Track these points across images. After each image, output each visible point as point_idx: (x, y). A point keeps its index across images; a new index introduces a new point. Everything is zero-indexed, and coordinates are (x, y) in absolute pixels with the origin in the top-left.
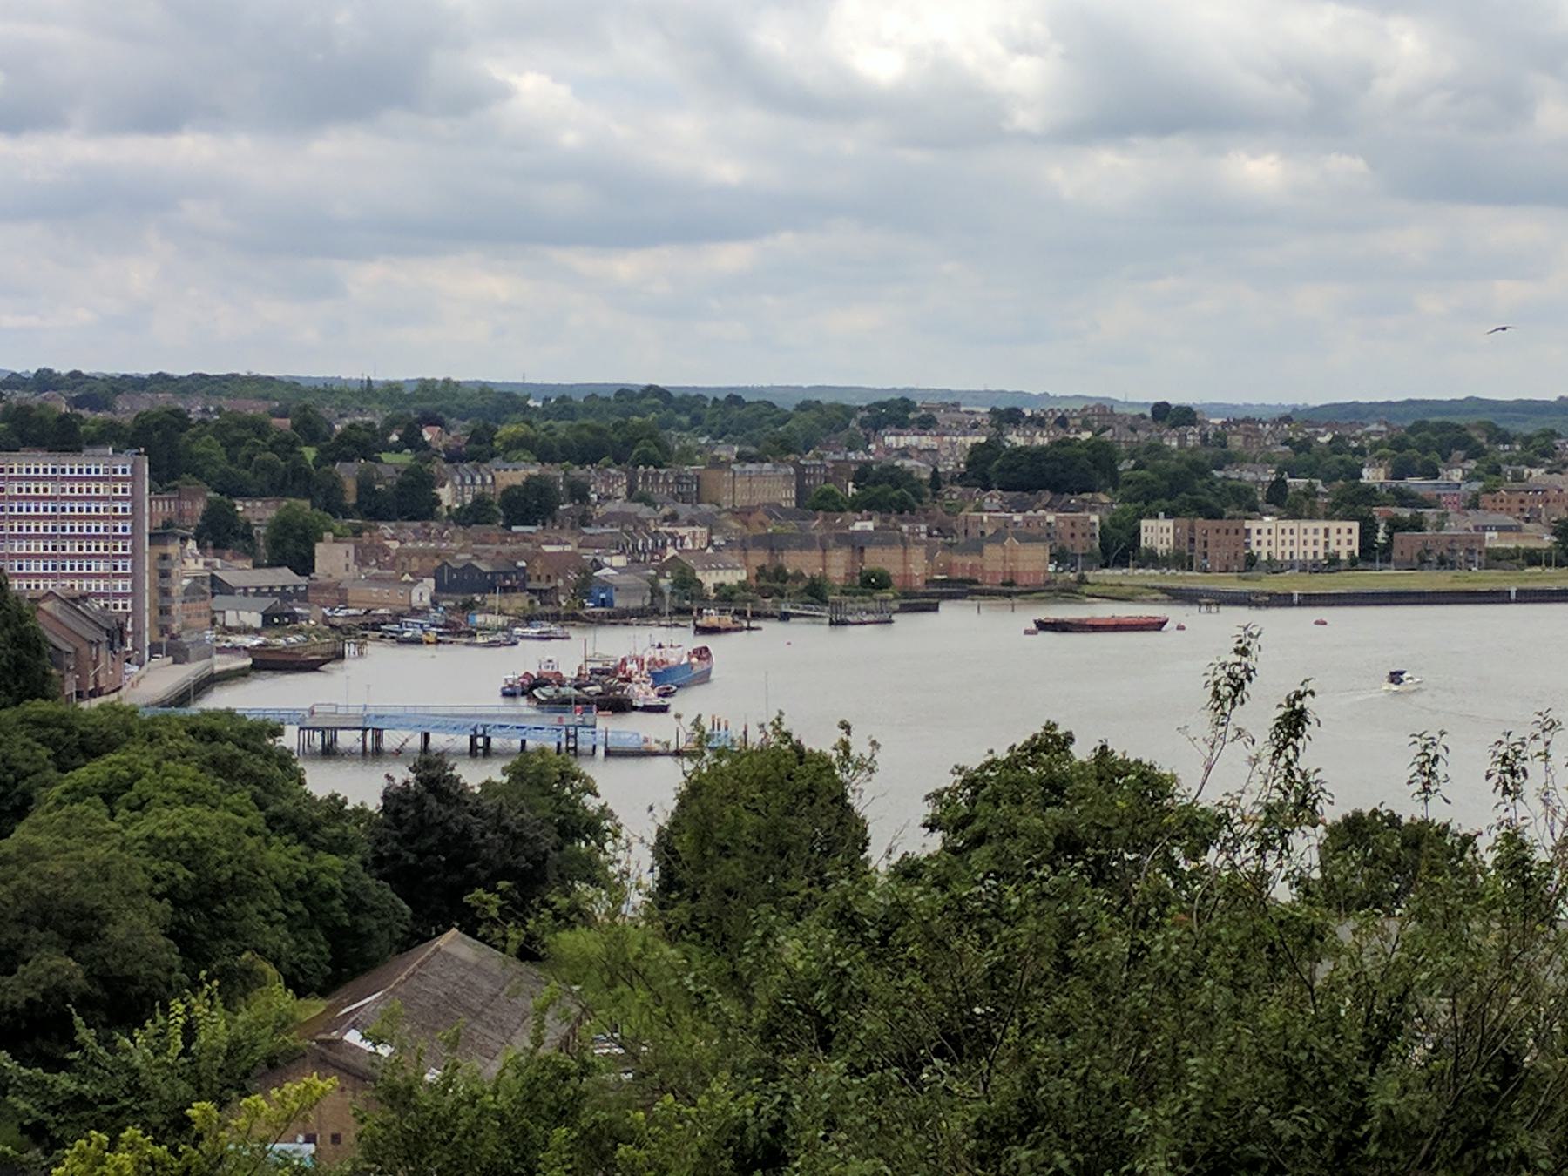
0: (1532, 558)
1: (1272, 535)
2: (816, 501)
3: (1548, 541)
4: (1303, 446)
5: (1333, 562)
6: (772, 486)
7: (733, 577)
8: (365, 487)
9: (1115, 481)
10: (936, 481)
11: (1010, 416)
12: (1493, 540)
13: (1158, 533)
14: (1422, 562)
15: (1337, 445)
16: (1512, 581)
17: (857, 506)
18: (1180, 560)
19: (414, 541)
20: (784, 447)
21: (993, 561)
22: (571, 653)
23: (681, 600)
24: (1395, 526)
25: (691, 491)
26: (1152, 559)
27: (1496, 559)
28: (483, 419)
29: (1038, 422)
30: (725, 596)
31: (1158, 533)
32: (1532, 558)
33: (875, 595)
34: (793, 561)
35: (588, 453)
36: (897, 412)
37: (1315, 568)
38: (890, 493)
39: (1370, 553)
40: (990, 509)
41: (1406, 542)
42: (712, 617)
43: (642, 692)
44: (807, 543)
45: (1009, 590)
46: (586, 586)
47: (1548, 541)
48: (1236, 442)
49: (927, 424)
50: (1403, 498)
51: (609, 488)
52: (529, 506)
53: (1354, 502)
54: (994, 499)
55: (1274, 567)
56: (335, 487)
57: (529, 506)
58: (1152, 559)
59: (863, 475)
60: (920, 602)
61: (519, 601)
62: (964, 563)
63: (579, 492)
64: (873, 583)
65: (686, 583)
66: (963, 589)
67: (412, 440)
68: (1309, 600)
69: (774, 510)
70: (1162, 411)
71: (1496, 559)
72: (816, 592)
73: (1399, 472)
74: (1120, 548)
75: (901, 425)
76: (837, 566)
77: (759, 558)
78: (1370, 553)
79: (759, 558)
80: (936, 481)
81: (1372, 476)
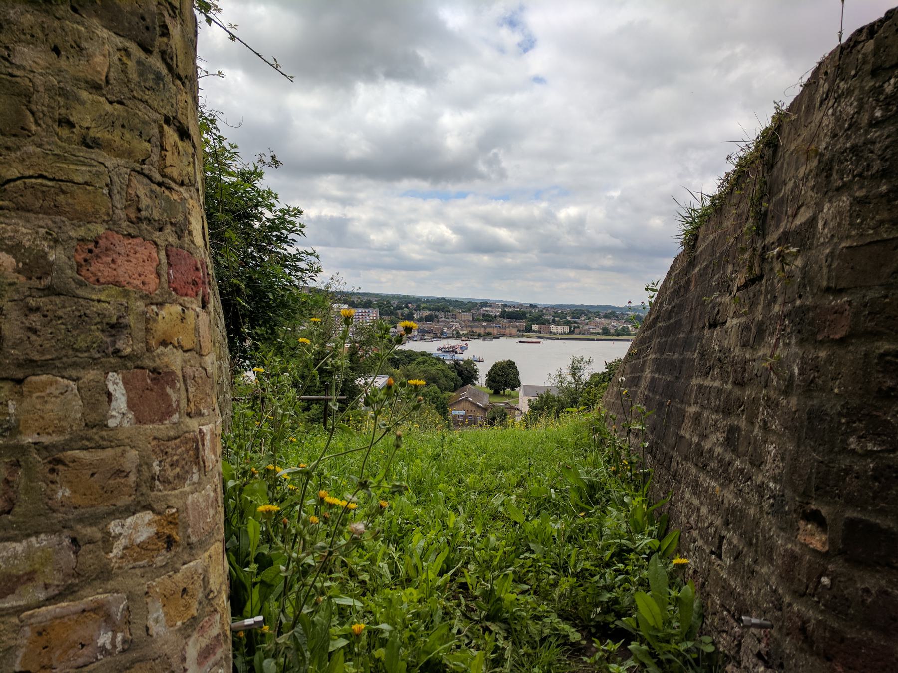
0: (598, 334)
1: (554, 328)
2: (475, 319)
3: (600, 331)
4: (556, 312)
5: (565, 333)
6: (468, 316)
7: (465, 332)
8: (402, 315)
9: (526, 318)
10: (496, 316)
11: (505, 305)
12: (591, 330)
13: (535, 327)
14: (580, 333)
15: (562, 312)
16: (595, 337)
17: (483, 320)
18: (539, 332)
19: (761, 286)
20: (470, 310)
21: (508, 331)
22: (334, 388)
23: (458, 336)
24: (575, 327)
25: (454, 317)
26: (534, 331)
27: (592, 333)
28: (418, 303)
29: (510, 306)
30: (465, 335)
31: (535, 327)
32: (598, 334)
33: (488, 336)
34: (475, 329)
35: (437, 310)
36: (485, 304)
37: (561, 334)
38: (488, 318)
39: (571, 332)
40: (505, 322)
41: (577, 330)
42: (464, 338)
43: (459, 351)
44: (477, 327)
45: (511, 336)
46: (442, 333)
47: (600, 331)
48: (544, 311)
49: (491, 306)
50: (575, 322)
51: (441, 315)
52: (429, 319)
53: (567, 323)
54: (505, 320)
55: (555, 333)
56: (397, 314)
57: (429, 319)
58: (534, 331)
59: (484, 315)
60: (497, 337)
61: (431, 335)
62: (503, 331)
63: (437, 316)
64: (489, 334)
65: (458, 333)
66: (503, 335)
67: (407, 306)
68: (562, 339)
69: (469, 320)
70: (531, 305)
71: (592, 333)
72: (480, 335)
73: (573, 318)
74: (529, 329)
75: (486, 306)
76: (482, 331)
77: (469, 329)
78: (571, 332)
79: (469, 329)
80: (496, 316)
81: (568, 318)
